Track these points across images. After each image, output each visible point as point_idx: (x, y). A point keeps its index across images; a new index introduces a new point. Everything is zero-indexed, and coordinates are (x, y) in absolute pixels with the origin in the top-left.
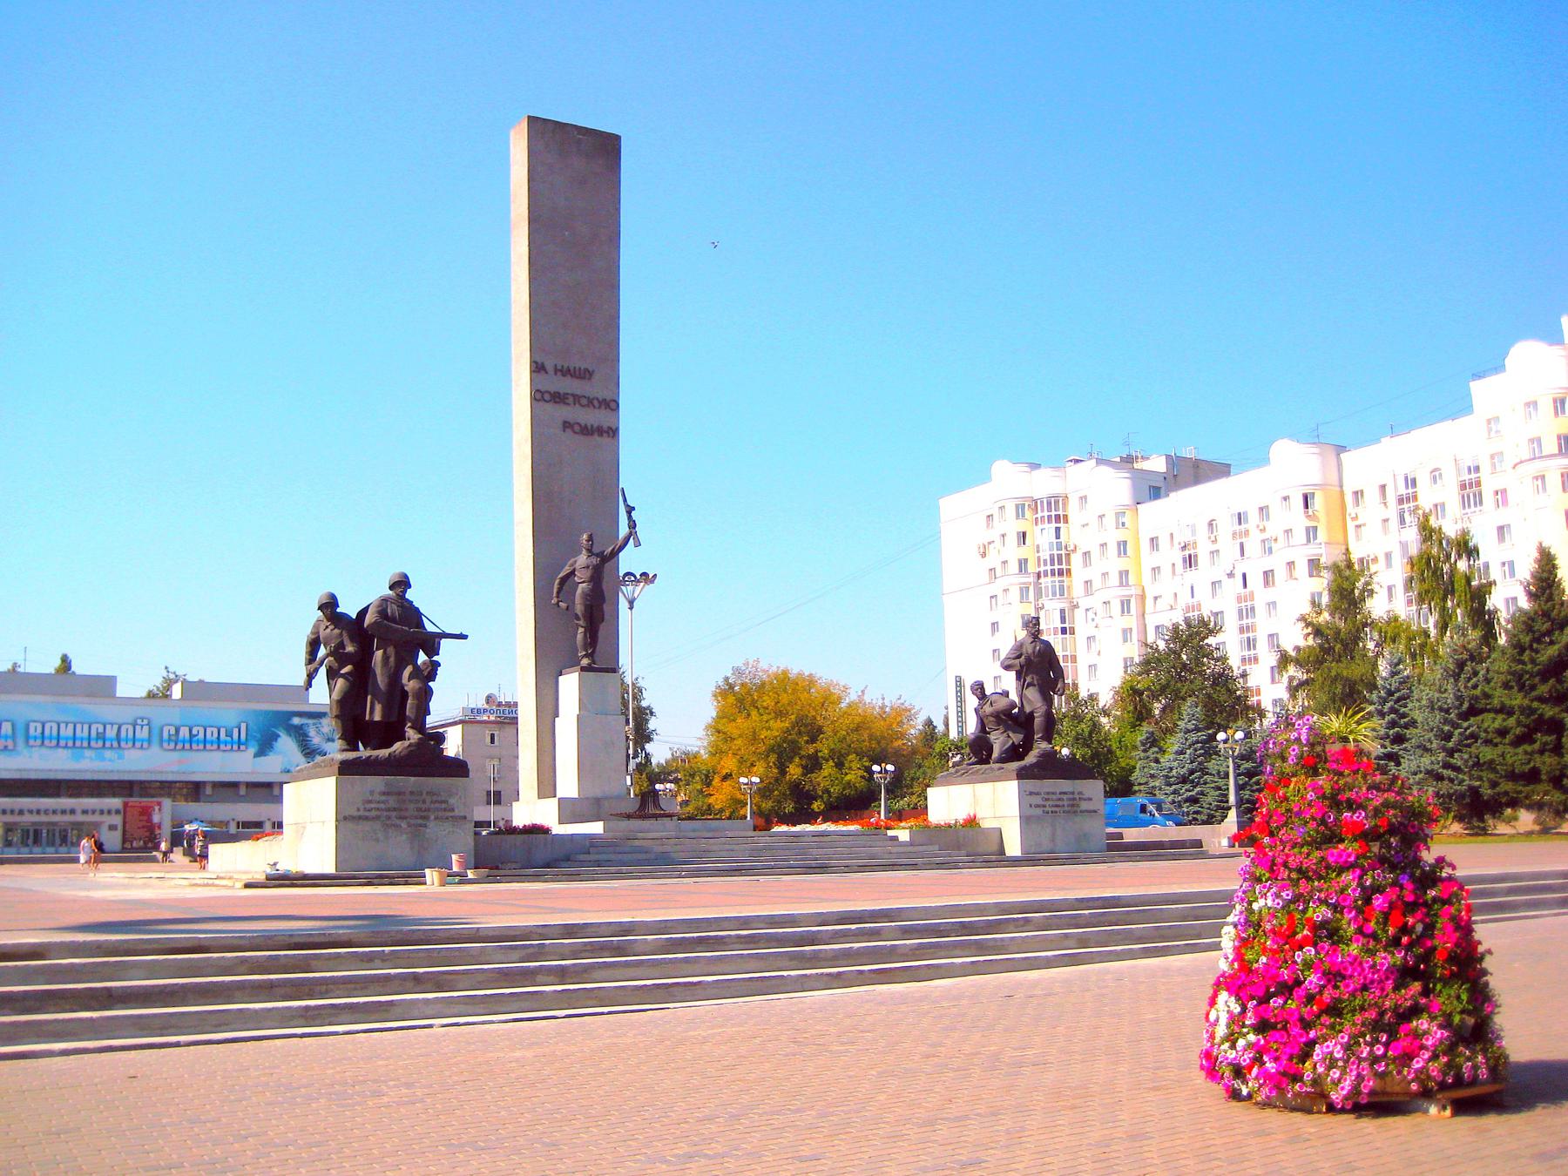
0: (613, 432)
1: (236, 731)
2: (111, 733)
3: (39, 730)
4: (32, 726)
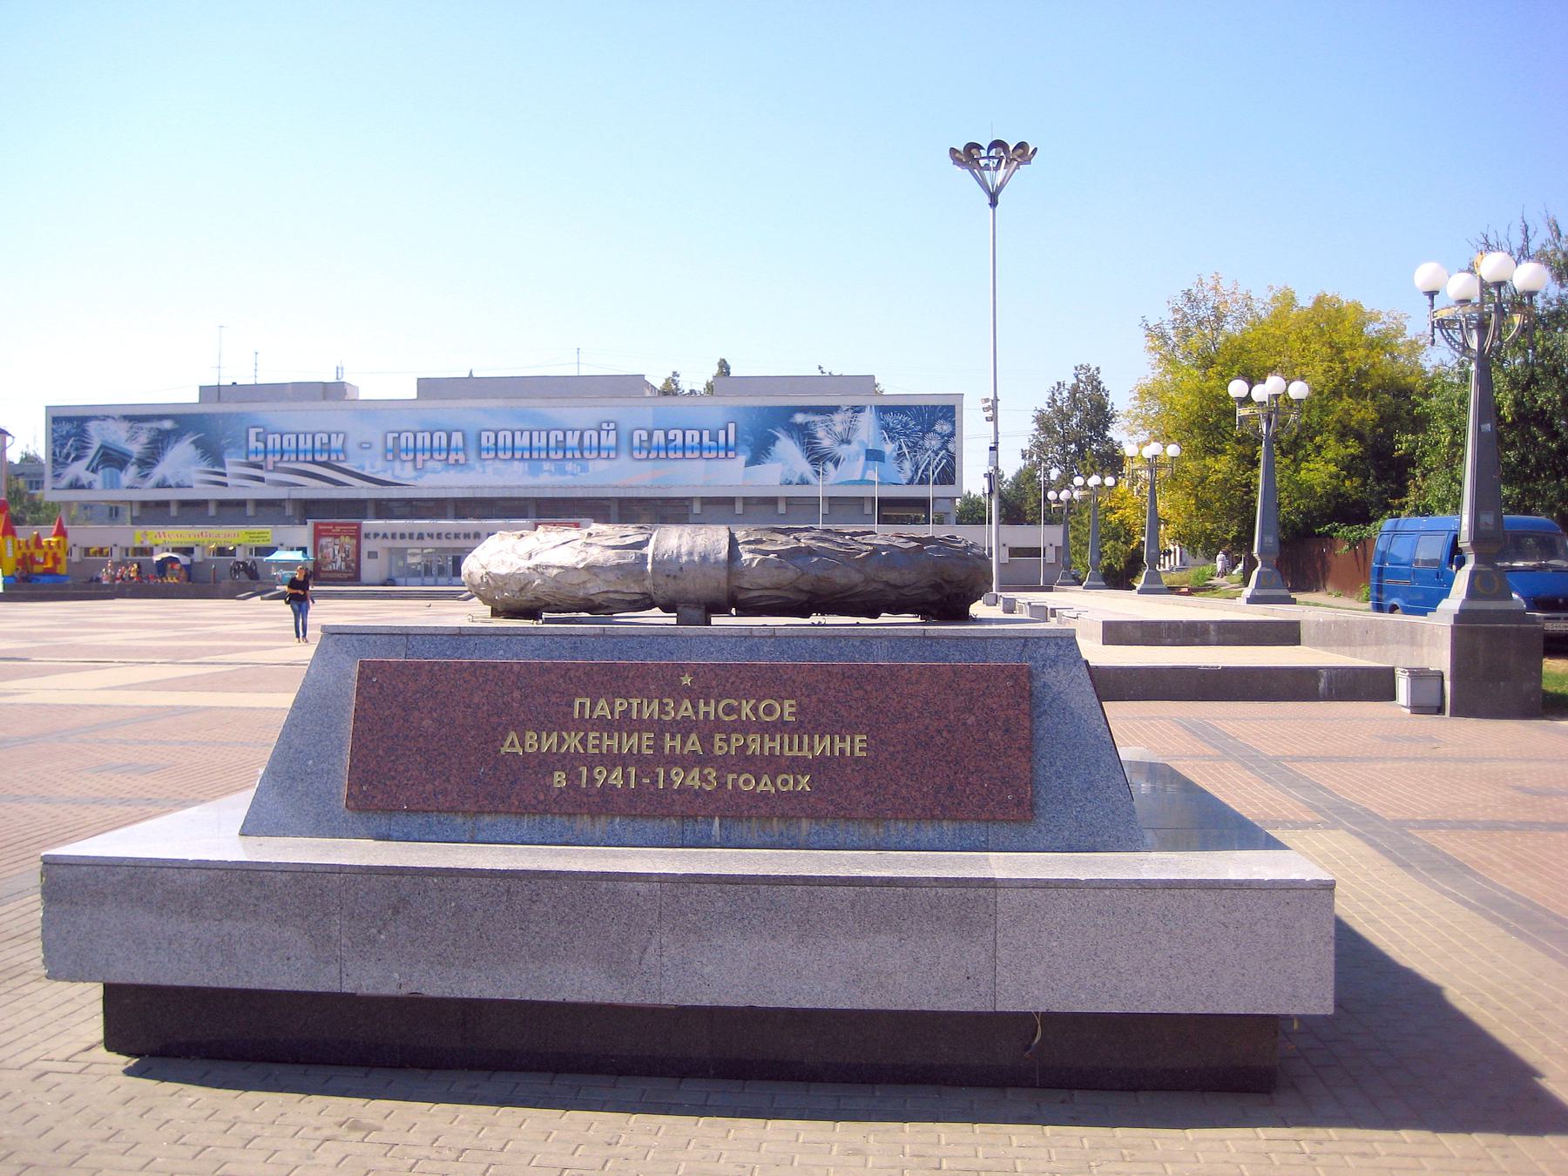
1: (722, 434)
2: (572, 441)
3: (492, 440)
4: (485, 435)
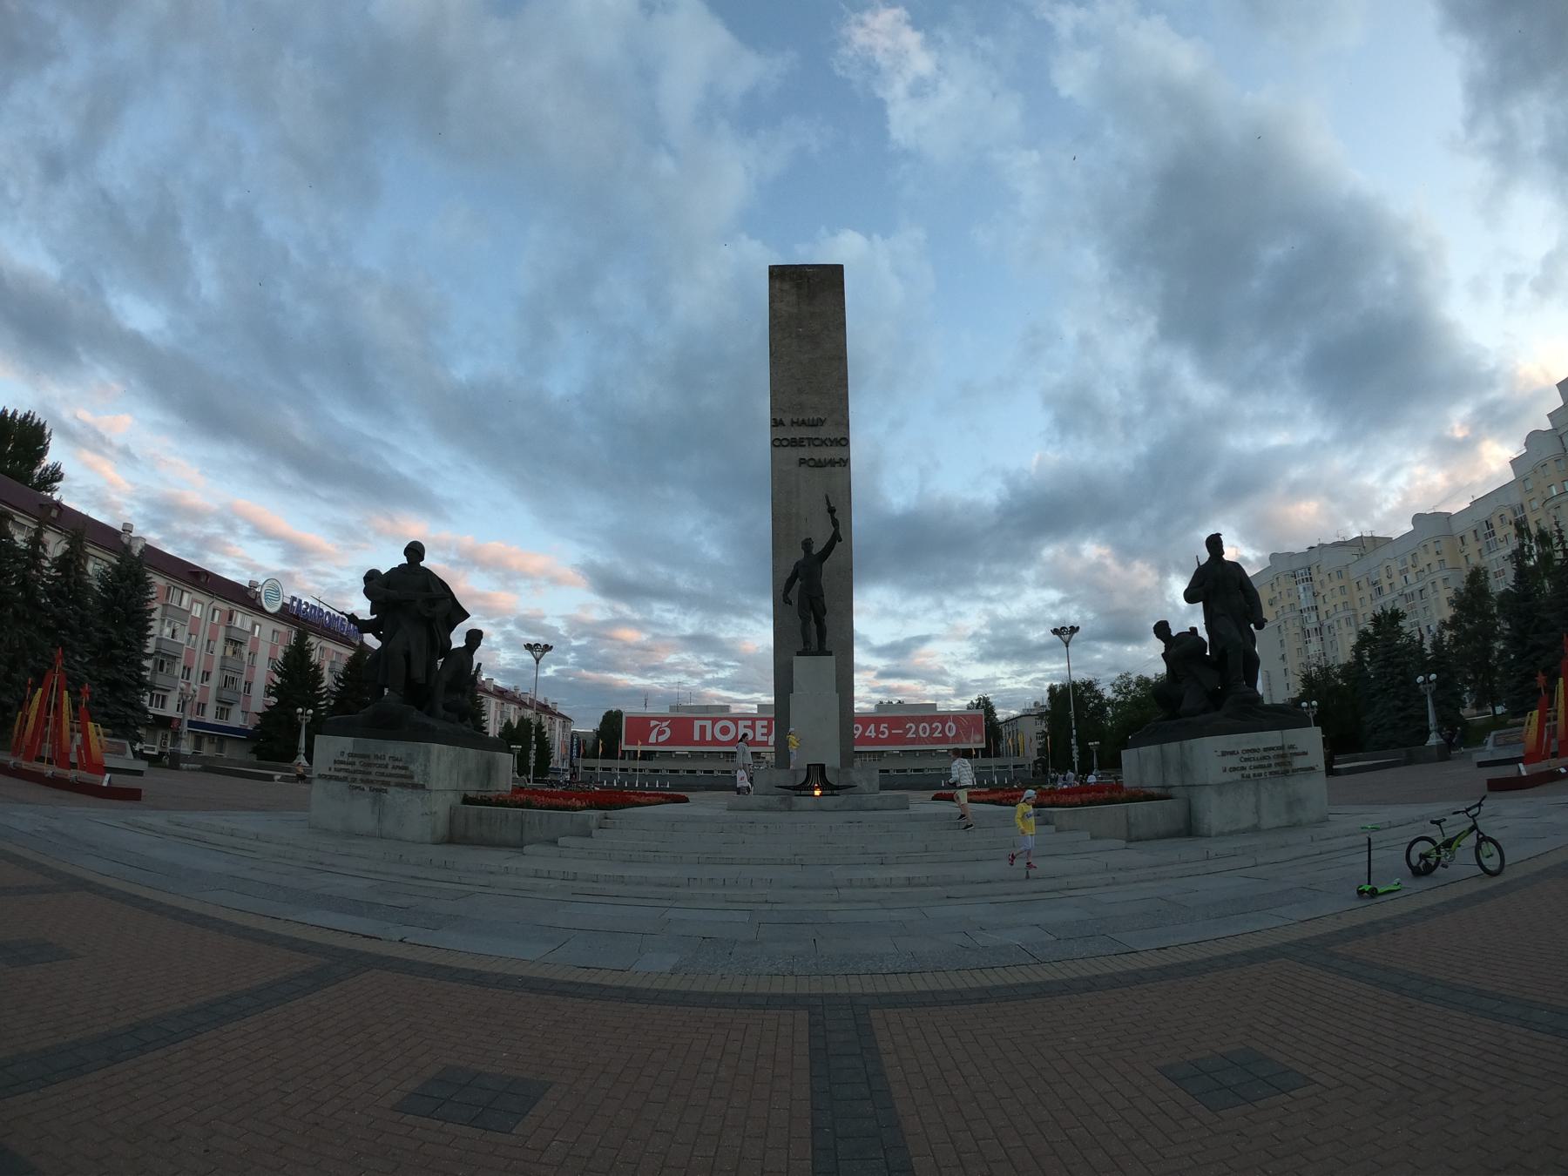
0: (845, 462)
